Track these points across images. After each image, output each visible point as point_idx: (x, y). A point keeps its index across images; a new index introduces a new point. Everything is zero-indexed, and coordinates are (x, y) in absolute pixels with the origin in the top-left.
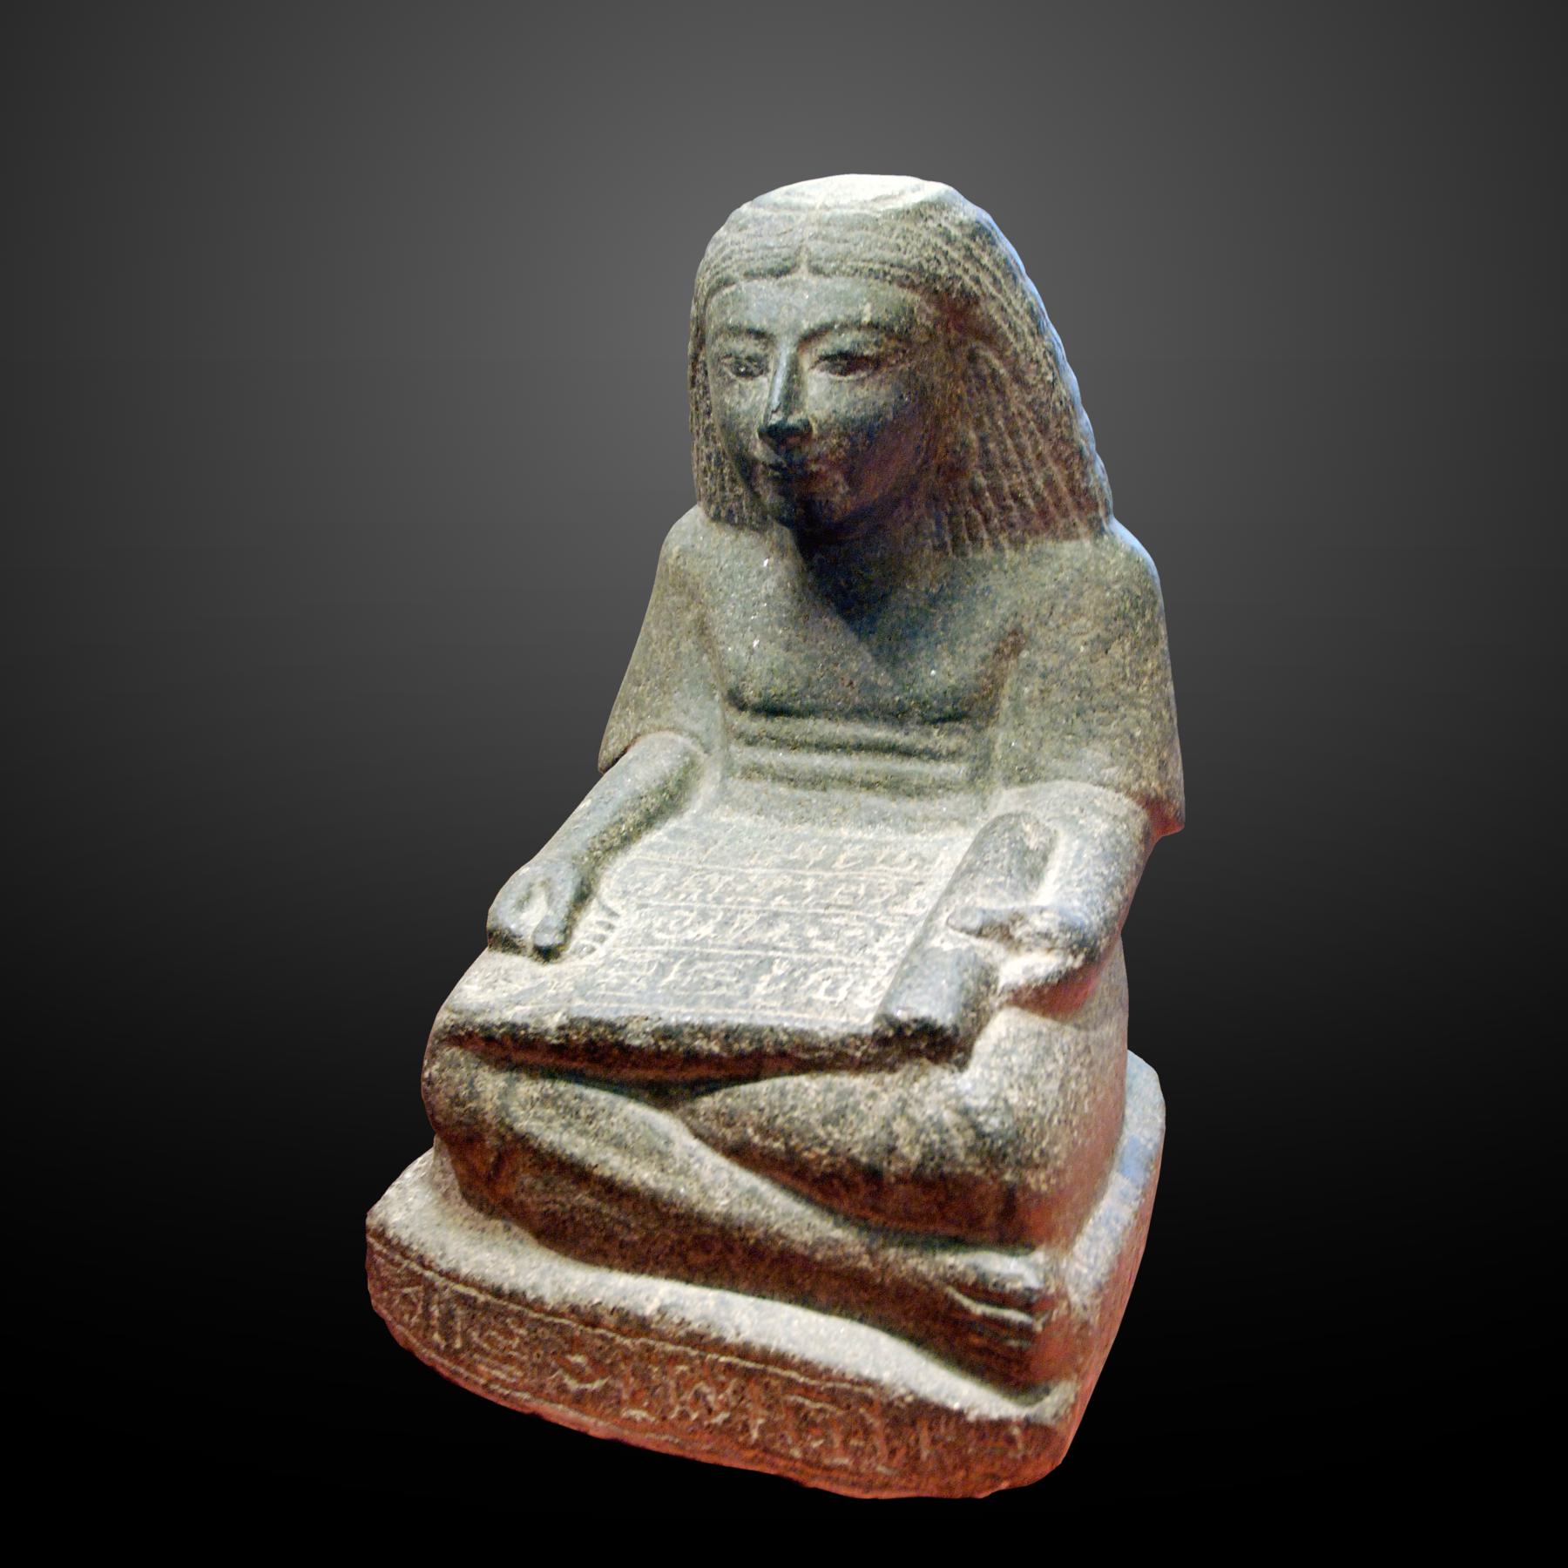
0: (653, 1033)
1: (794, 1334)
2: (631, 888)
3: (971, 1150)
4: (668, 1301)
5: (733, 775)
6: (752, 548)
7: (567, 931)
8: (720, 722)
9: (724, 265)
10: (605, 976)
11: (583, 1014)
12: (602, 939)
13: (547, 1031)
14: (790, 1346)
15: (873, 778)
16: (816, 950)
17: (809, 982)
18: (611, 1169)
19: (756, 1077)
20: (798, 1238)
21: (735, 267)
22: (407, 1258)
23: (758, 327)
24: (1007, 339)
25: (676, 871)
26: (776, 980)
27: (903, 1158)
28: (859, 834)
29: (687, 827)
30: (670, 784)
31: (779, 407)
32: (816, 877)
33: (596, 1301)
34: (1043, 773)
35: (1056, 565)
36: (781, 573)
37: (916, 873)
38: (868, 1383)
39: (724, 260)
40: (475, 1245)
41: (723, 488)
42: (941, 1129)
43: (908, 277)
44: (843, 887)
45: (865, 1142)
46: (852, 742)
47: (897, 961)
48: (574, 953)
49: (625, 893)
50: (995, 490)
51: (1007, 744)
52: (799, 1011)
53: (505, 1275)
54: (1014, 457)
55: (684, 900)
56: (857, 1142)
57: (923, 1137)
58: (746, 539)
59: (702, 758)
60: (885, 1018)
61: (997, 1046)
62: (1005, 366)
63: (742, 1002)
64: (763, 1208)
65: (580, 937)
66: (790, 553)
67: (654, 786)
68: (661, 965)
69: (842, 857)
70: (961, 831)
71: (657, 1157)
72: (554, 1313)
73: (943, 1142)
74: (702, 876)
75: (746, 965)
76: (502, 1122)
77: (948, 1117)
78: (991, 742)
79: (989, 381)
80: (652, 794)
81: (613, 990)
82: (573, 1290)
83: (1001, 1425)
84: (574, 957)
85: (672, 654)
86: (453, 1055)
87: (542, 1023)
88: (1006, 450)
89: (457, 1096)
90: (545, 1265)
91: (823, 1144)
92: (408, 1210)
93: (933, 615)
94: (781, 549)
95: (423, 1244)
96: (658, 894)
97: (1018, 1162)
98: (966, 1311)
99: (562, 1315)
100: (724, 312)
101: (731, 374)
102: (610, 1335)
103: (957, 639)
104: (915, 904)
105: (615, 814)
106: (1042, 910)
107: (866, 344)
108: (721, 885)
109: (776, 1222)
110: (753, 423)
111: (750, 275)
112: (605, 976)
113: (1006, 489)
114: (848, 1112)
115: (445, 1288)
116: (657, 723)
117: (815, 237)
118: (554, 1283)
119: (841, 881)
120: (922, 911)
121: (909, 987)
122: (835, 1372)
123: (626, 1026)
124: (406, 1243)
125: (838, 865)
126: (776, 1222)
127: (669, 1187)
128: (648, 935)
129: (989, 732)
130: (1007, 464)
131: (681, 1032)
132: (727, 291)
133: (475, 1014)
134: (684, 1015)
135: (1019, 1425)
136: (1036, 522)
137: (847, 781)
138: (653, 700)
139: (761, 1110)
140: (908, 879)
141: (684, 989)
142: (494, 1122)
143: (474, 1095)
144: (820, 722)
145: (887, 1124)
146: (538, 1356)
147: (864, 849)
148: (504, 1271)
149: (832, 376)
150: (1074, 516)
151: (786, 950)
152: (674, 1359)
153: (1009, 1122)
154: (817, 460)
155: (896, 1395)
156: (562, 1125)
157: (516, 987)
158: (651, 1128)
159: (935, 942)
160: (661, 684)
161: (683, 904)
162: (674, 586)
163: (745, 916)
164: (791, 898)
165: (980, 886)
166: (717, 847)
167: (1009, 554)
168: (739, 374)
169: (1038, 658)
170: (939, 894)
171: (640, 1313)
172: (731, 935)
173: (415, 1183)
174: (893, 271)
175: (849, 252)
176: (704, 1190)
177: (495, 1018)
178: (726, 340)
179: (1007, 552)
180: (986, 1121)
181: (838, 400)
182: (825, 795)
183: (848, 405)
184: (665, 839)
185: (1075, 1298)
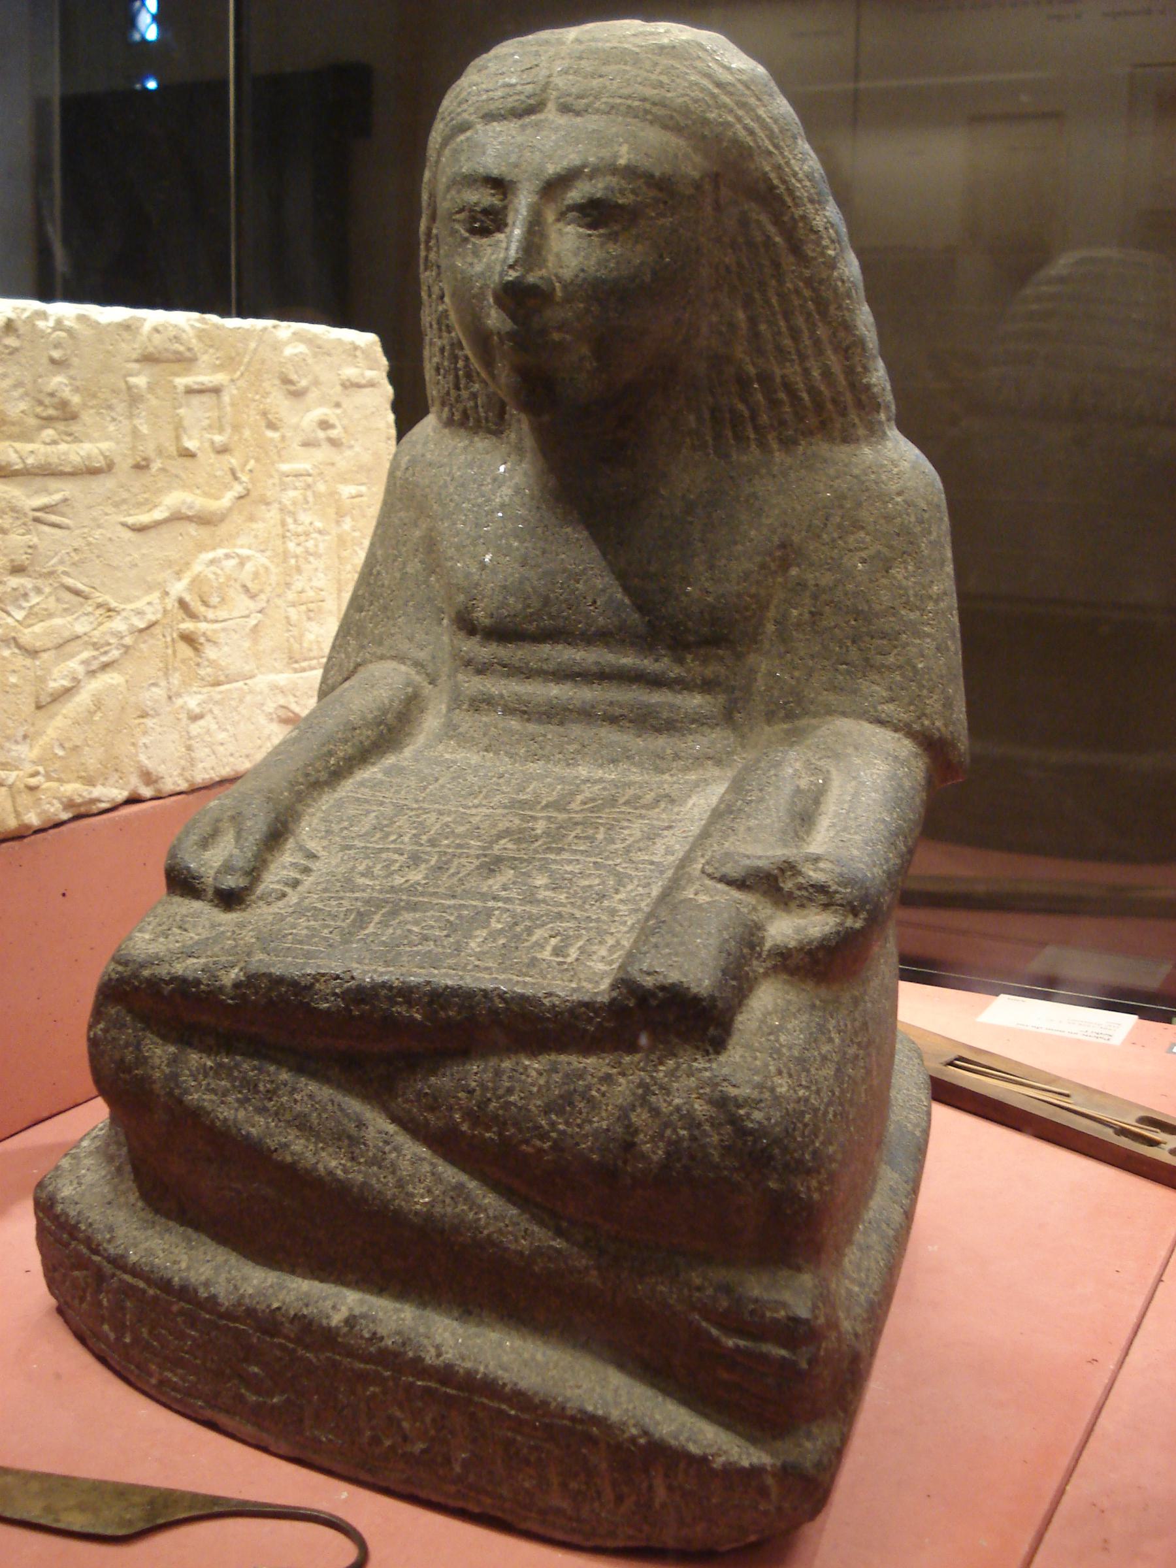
0: (344, 995)
1: (505, 1358)
2: (335, 827)
3: (727, 1150)
4: (357, 1312)
5: (459, 707)
6: (487, 453)
7: (254, 873)
8: (448, 648)
9: (459, 110)
10: (294, 926)
11: (264, 970)
12: (295, 884)
13: (221, 988)
14: (500, 1372)
15: (618, 711)
16: (544, 901)
17: (534, 938)
18: (293, 1154)
19: (464, 1053)
20: (513, 1247)
21: (472, 110)
22: (74, 1238)
23: (495, 172)
24: (784, 203)
25: (388, 810)
26: (494, 935)
27: (644, 1157)
28: (600, 773)
29: (406, 763)
30: (389, 716)
31: (516, 261)
32: (549, 818)
33: (275, 1305)
34: (812, 708)
35: (832, 472)
36: (518, 479)
37: (664, 816)
38: (594, 1419)
39: (460, 104)
40: (146, 1229)
41: (457, 388)
42: (692, 1122)
43: (671, 117)
44: (578, 830)
45: (596, 1134)
46: (594, 669)
47: (640, 916)
48: (260, 898)
49: (328, 832)
50: (765, 378)
51: (770, 674)
52: (520, 974)
53: (176, 1267)
54: (787, 342)
55: (394, 842)
56: (586, 1136)
57: (668, 1132)
58: (482, 443)
59: (427, 689)
60: (625, 984)
61: (763, 1022)
62: (781, 234)
63: (451, 961)
64: (471, 1209)
65: (271, 879)
66: (529, 455)
67: (370, 716)
68: (360, 914)
69: (579, 798)
70: (716, 772)
71: (346, 1142)
72: (229, 1315)
73: (693, 1139)
74: (418, 816)
75: (460, 917)
76: (170, 1094)
77: (700, 1108)
78: (753, 671)
79: (762, 250)
80: (367, 725)
81: (301, 942)
82: (250, 1291)
83: (755, 1472)
84: (261, 903)
85: (398, 575)
86: (117, 1013)
87: (217, 978)
88: (779, 333)
89: (122, 1060)
90: (220, 1259)
91: (544, 1137)
92: (80, 1184)
93: (691, 523)
94: (519, 450)
95: (91, 1225)
96: (366, 834)
97: (786, 1166)
98: (716, 1342)
99: (236, 1319)
100: (458, 161)
101: (463, 232)
102: (291, 1346)
103: (717, 550)
104: (663, 852)
105: (324, 745)
106: (817, 859)
107: (622, 192)
108: (438, 826)
109: (487, 1225)
110: (487, 286)
111: (490, 117)
112: (294, 926)
113: (778, 380)
114: (577, 1097)
115: (113, 1275)
116: (379, 651)
117: (565, 72)
118: (229, 1281)
119: (577, 824)
120: (671, 858)
121: (656, 946)
122: (553, 1404)
123: (312, 985)
124: (73, 1222)
125: (574, 806)
126: (487, 1225)
127: (360, 1178)
128: (349, 880)
129: (752, 659)
130: (780, 350)
131: (377, 995)
132: (462, 137)
133: (142, 966)
134: (381, 974)
135: (774, 1475)
136: (812, 421)
137: (586, 714)
138: (376, 626)
139: (471, 1092)
140: (655, 822)
141: (384, 943)
142: (163, 1093)
143: (142, 1061)
144: (560, 647)
145: (624, 1114)
146: (212, 1360)
147: (604, 789)
148: (175, 1262)
149: (581, 230)
150: (853, 416)
151: (507, 900)
152: (363, 1378)
153: (776, 1115)
154: (559, 329)
155: (626, 1435)
156: (238, 1100)
157: (192, 936)
158: (342, 1110)
159: (689, 894)
160: (385, 608)
161: (392, 846)
162: (400, 500)
163: (463, 861)
164: (519, 841)
165: (742, 828)
166: (437, 785)
167: (778, 456)
168: (473, 231)
169: (810, 577)
170: (691, 839)
171: (324, 1322)
172: (445, 880)
173: (91, 1153)
174: (655, 110)
175: (605, 87)
176: (400, 1184)
177: (163, 971)
178: (459, 192)
179: (777, 454)
180: (748, 1115)
181: (586, 258)
182: (561, 729)
183: (599, 263)
184: (380, 776)
185: (846, 1325)
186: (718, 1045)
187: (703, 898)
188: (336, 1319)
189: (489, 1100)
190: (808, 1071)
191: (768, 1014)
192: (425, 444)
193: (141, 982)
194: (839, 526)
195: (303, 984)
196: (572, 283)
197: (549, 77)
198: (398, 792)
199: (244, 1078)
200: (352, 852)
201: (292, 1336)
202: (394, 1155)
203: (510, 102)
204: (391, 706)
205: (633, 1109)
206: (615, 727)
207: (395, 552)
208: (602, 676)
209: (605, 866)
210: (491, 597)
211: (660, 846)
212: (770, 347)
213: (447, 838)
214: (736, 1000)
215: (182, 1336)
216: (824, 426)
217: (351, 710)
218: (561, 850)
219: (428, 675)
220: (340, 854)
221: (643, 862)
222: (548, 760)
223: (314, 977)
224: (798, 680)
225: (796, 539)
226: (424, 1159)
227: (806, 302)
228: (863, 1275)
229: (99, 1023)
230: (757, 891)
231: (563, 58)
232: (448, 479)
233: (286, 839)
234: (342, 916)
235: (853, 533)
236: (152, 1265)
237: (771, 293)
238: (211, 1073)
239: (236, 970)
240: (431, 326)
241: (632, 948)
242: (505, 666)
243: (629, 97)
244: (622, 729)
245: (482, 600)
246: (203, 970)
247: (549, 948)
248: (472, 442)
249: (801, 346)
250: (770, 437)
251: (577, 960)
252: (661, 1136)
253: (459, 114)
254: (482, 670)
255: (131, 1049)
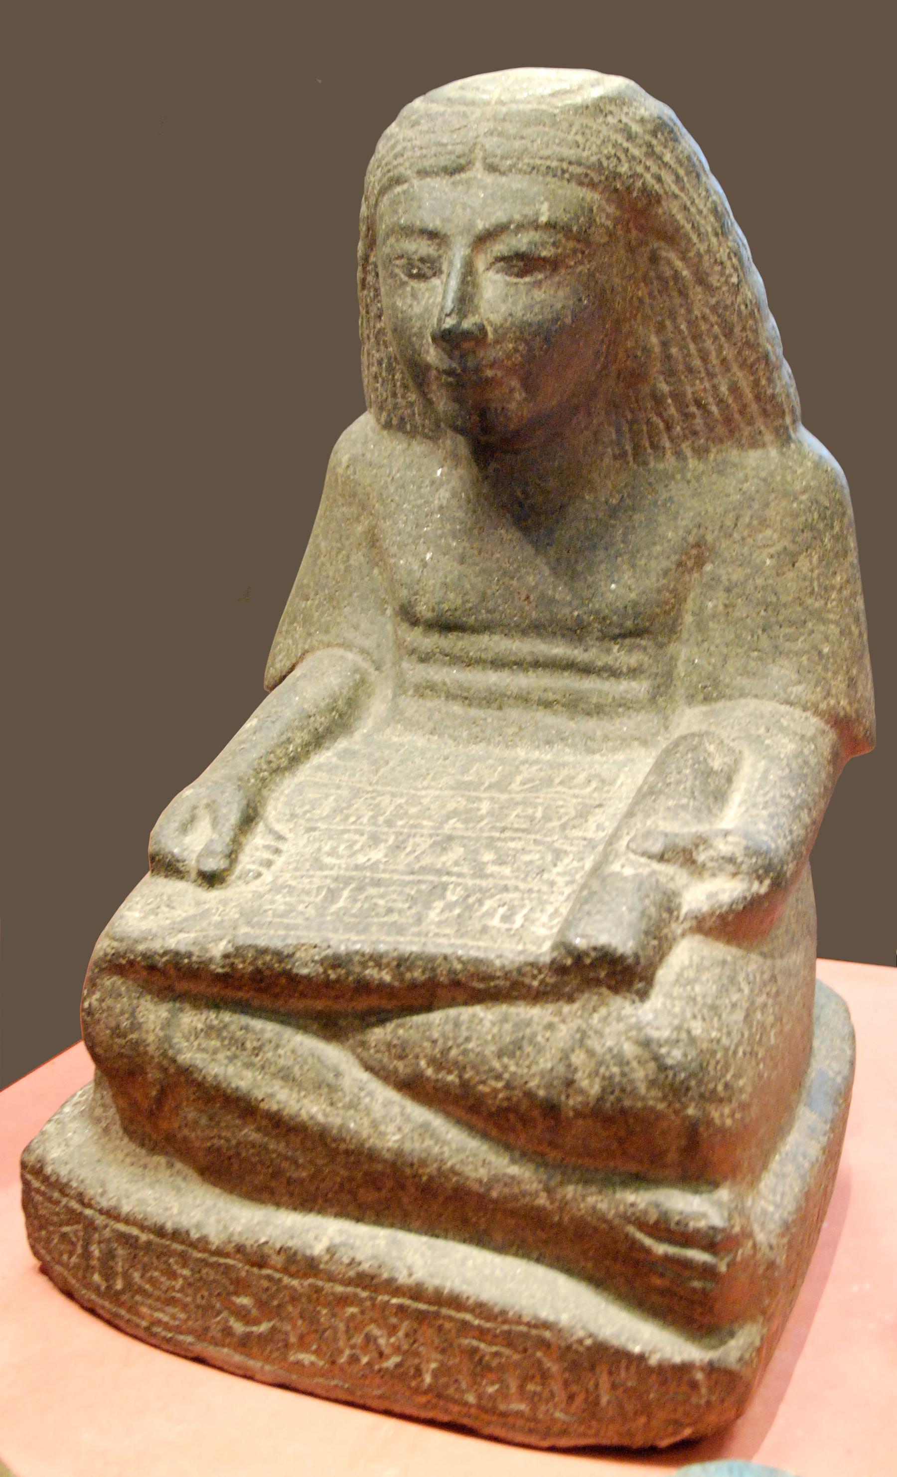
0: (322, 962)
2: (299, 811)
3: (652, 1083)
4: (337, 1240)
7: (232, 856)
9: (395, 163)
12: (269, 864)
13: (211, 960)
15: (551, 696)
16: (492, 875)
17: (485, 908)
18: (278, 1103)
20: (473, 1175)
21: (407, 164)
23: (431, 226)
26: (450, 906)
27: (582, 1091)
28: (537, 754)
29: (357, 747)
30: (340, 702)
32: (492, 799)
33: (263, 1240)
34: (728, 691)
35: (741, 475)
36: (455, 483)
37: (595, 795)
38: (545, 1325)
39: (395, 157)
40: (137, 1182)
41: (394, 395)
42: (621, 1061)
43: (587, 175)
44: (519, 810)
45: (542, 1074)
46: (529, 658)
47: (575, 887)
48: (239, 878)
49: (293, 816)
50: (678, 397)
52: (474, 938)
53: (168, 1213)
55: (354, 823)
56: (534, 1075)
58: (419, 447)
59: (373, 675)
63: (415, 929)
64: (436, 1143)
65: (246, 861)
66: (464, 462)
69: (519, 779)
70: (642, 751)
71: (326, 1090)
72: (219, 1253)
73: (623, 1074)
75: (419, 891)
76: (164, 1054)
77: (629, 1049)
78: (673, 659)
79: (671, 283)
80: (321, 713)
81: (281, 916)
84: (240, 882)
85: (342, 567)
86: (113, 984)
87: (207, 951)
88: (689, 355)
89: (118, 1026)
90: (209, 1202)
92: (67, 1145)
93: (614, 526)
96: (327, 816)
97: (702, 1096)
98: (648, 1251)
99: (227, 1255)
101: (402, 276)
102: (277, 1275)
103: (638, 551)
105: (282, 734)
106: (726, 834)
107: (544, 244)
108: (392, 808)
109: (450, 1157)
111: (423, 173)
114: (525, 1043)
115: (106, 1226)
116: (326, 638)
117: (491, 133)
118: (218, 1221)
119: (517, 804)
121: (589, 913)
122: (511, 1314)
123: (294, 954)
125: (514, 786)
128: (317, 860)
129: (672, 648)
130: (690, 370)
131: (351, 960)
132: (398, 189)
133: (137, 942)
134: (355, 943)
136: (721, 430)
137: (524, 699)
139: (434, 1042)
141: (354, 916)
142: (157, 1054)
143: (136, 1026)
144: (496, 638)
145: (565, 1056)
147: (541, 770)
148: (167, 1209)
149: (508, 278)
150: (760, 423)
151: (460, 875)
152: (344, 1301)
153: (692, 1053)
154: (492, 366)
155: (575, 1338)
156: (227, 1057)
157: (180, 914)
159: (616, 867)
160: (331, 598)
161: (353, 827)
162: (343, 496)
163: (418, 839)
164: (466, 821)
165: (662, 808)
166: (388, 768)
167: (692, 463)
168: (411, 276)
169: (723, 572)
171: (308, 1252)
173: (74, 1118)
174: (572, 169)
176: (375, 1124)
177: (157, 946)
178: (397, 240)
179: (690, 460)
180: (669, 1053)
181: (514, 303)
182: (500, 714)
184: (334, 760)
185: (761, 1237)
186: (643, 995)
187: (628, 871)
188: (318, 1249)
189: (450, 1048)
190: (720, 1017)
191: (683, 969)
192: (365, 443)
193: (136, 956)
194: (749, 525)
195: (286, 953)
196: (502, 325)
197: (477, 137)
198: (353, 775)
199: (231, 1038)
200: (317, 833)
201: (279, 1266)
202: (367, 1100)
203: (443, 161)
204: (341, 693)
205: (573, 1050)
206: (548, 711)
207: (339, 545)
208: (537, 664)
209: (543, 843)
210: (433, 592)
211: (592, 824)
212: (681, 367)
213: (401, 819)
214: (657, 958)
215: (173, 1275)
216: (733, 431)
217: (305, 698)
218: (503, 830)
219: (373, 662)
220: (306, 836)
221: (577, 838)
222: (489, 742)
223: (296, 946)
224: (714, 666)
225: (709, 538)
226: (394, 1102)
227: (712, 326)
228: (778, 1198)
229: (94, 993)
230: (675, 863)
231: (488, 120)
232: (389, 480)
233: (257, 824)
234: (314, 892)
235: (760, 531)
236: (145, 1213)
237: (680, 320)
238: (202, 1035)
239: (224, 942)
240: (369, 338)
241: (568, 915)
242: (446, 655)
243: (548, 158)
244: (555, 713)
245: (424, 595)
246: (194, 943)
247: (498, 917)
248: (409, 445)
249: (709, 366)
250: (684, 446)
251: (522, 926)
252: (597, 1073)
253: (396, 167)
254: (425, 659)
255: (126, 1016)
